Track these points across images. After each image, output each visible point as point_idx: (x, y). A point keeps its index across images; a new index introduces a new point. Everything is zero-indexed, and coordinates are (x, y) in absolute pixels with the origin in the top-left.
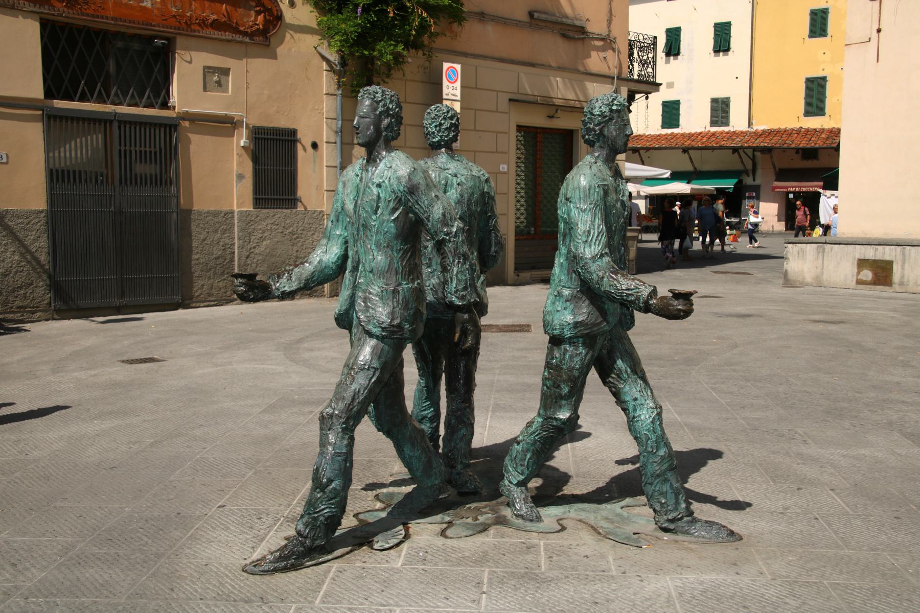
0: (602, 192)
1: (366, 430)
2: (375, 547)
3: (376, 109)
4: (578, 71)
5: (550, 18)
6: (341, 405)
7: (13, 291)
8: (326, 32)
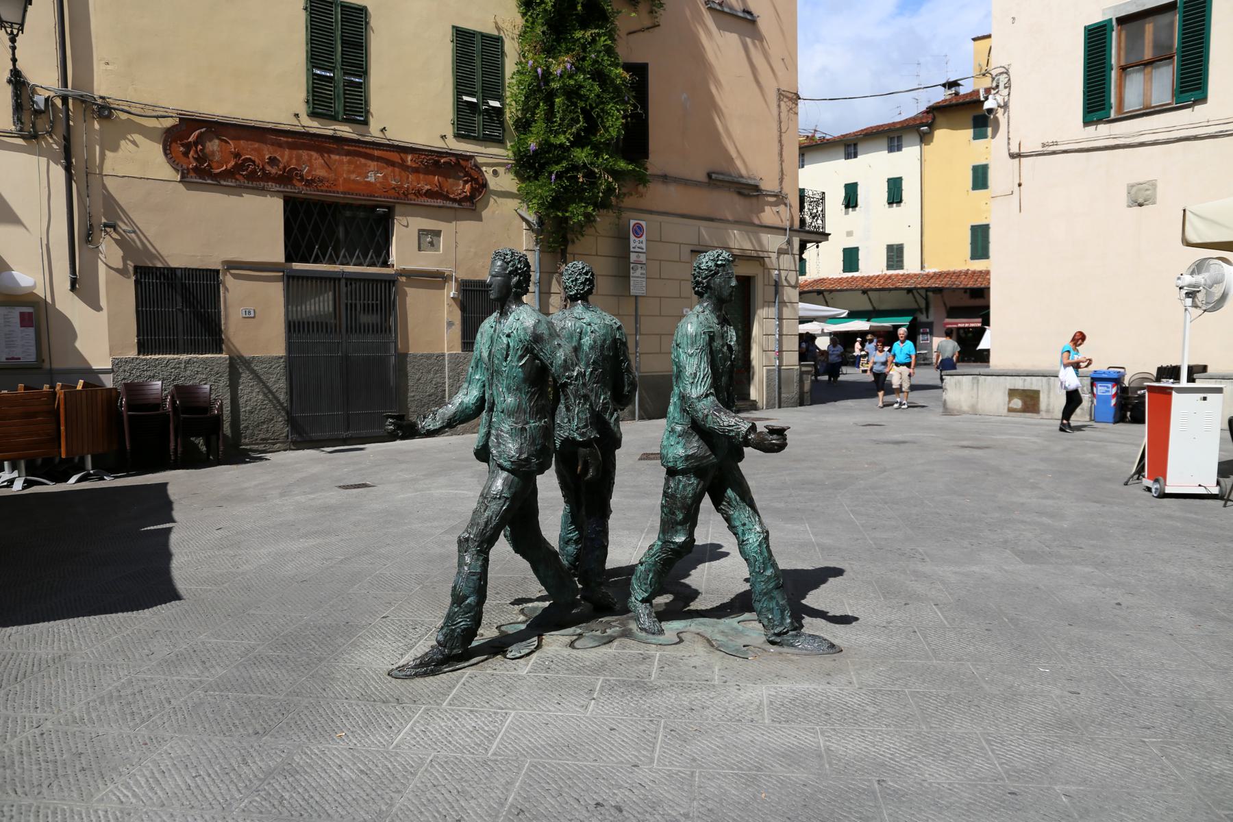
1: (502, 548)
3: (505, 269)
5: (727, 178)
7: (258, 426)
8: (525, 196)
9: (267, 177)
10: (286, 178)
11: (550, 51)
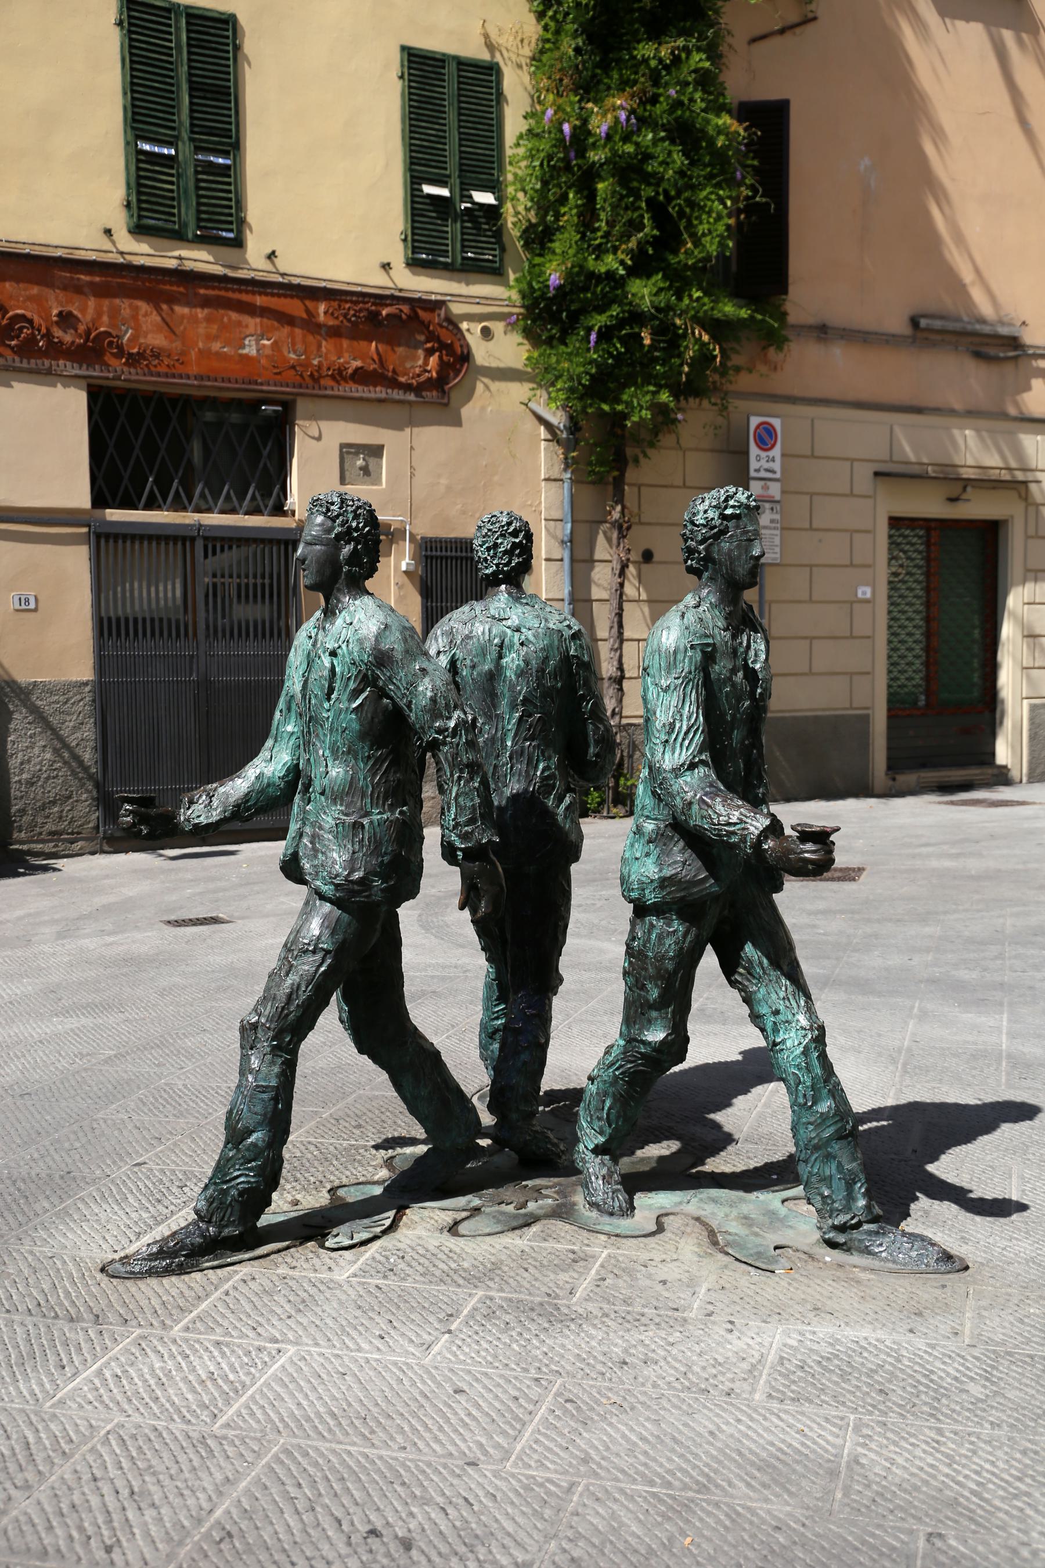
0: (699, 656)
2: (327, 1244)
3: (329, 531)
4: (1004, 416)
5: (950, 326)
6: (268, 1010)
7: (43, 808)
8: (542, 375)
9: (56, 350)
10: (92, 350)
11: (589, 88)
